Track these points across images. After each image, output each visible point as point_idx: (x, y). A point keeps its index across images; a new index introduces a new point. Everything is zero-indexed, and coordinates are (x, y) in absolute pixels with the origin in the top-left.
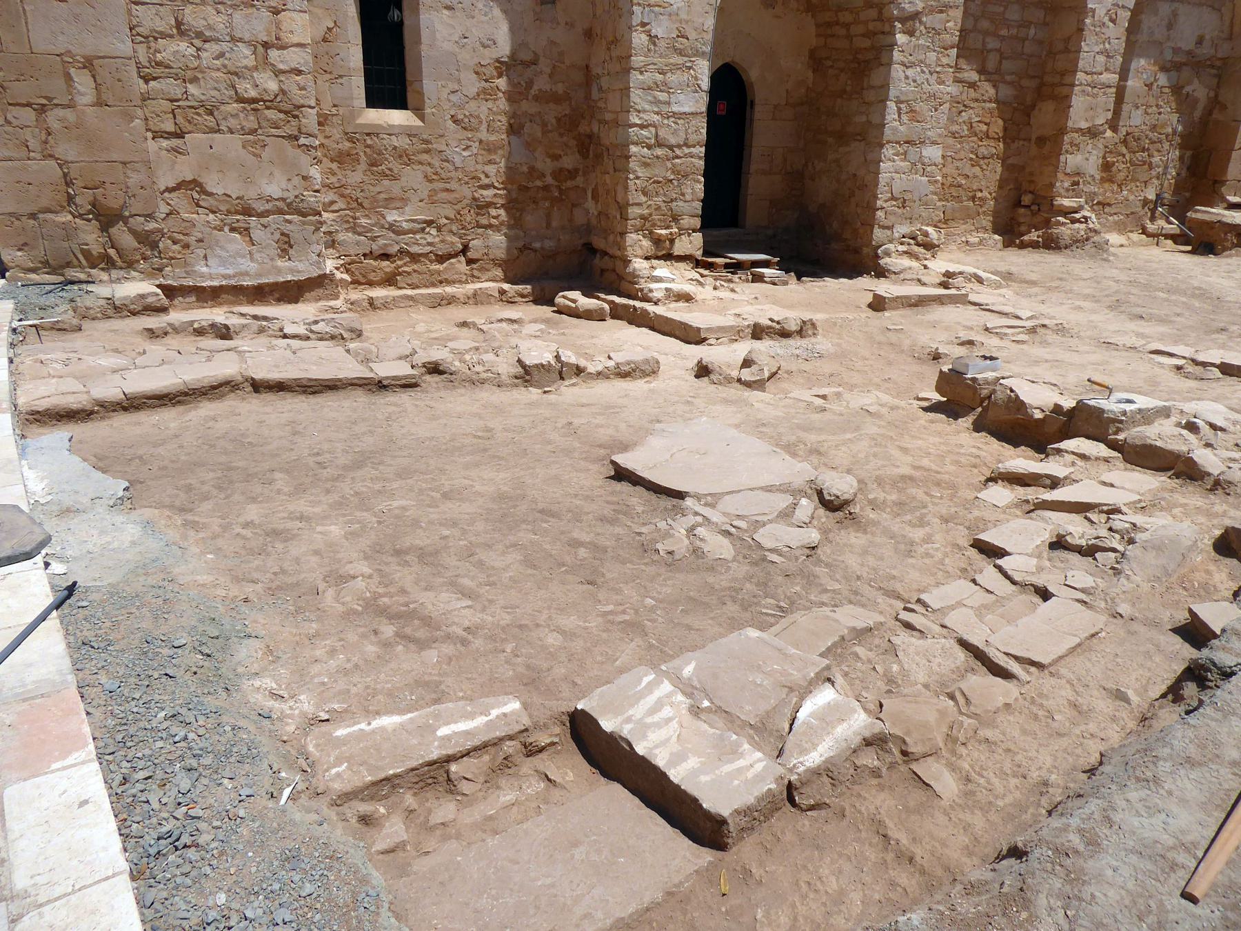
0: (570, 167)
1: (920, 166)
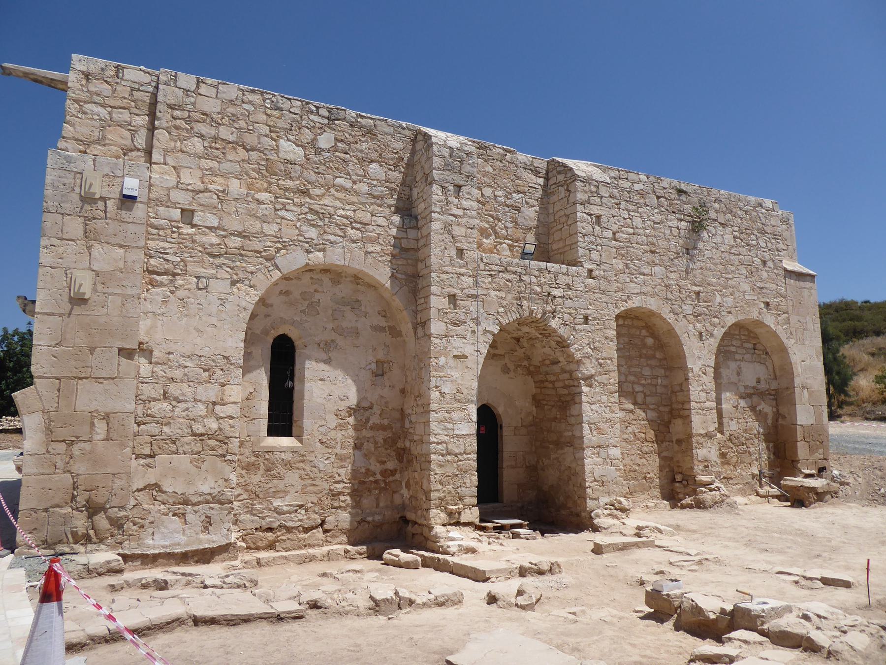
0: (391, 468)
1: (608, 460)
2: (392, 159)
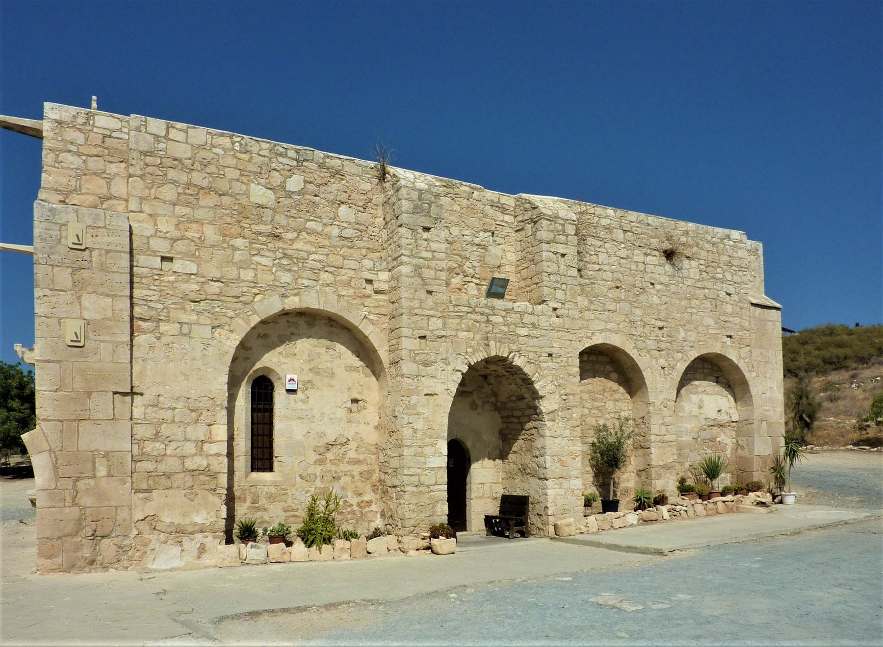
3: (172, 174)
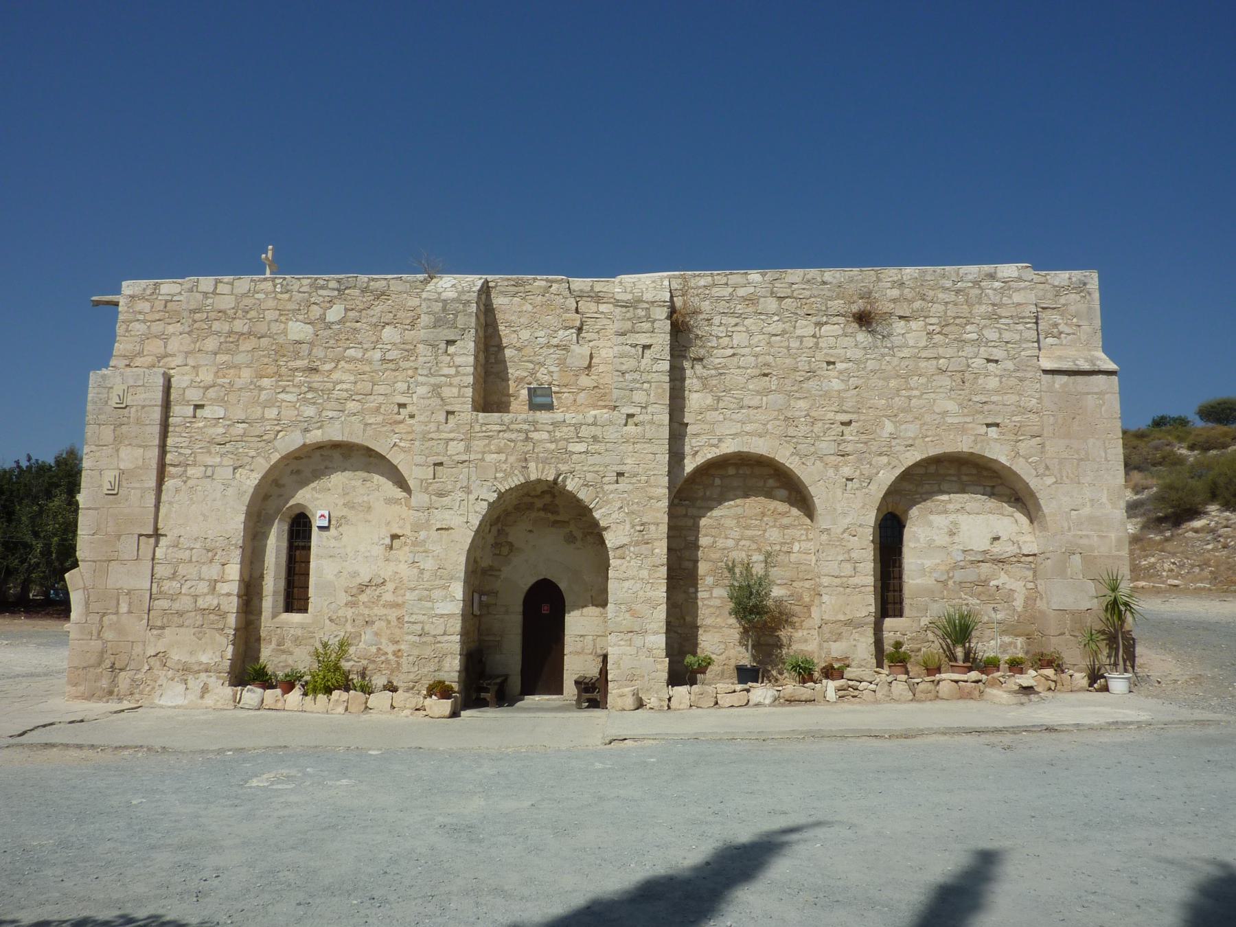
2: (407, 318)
3: (216, 326)
